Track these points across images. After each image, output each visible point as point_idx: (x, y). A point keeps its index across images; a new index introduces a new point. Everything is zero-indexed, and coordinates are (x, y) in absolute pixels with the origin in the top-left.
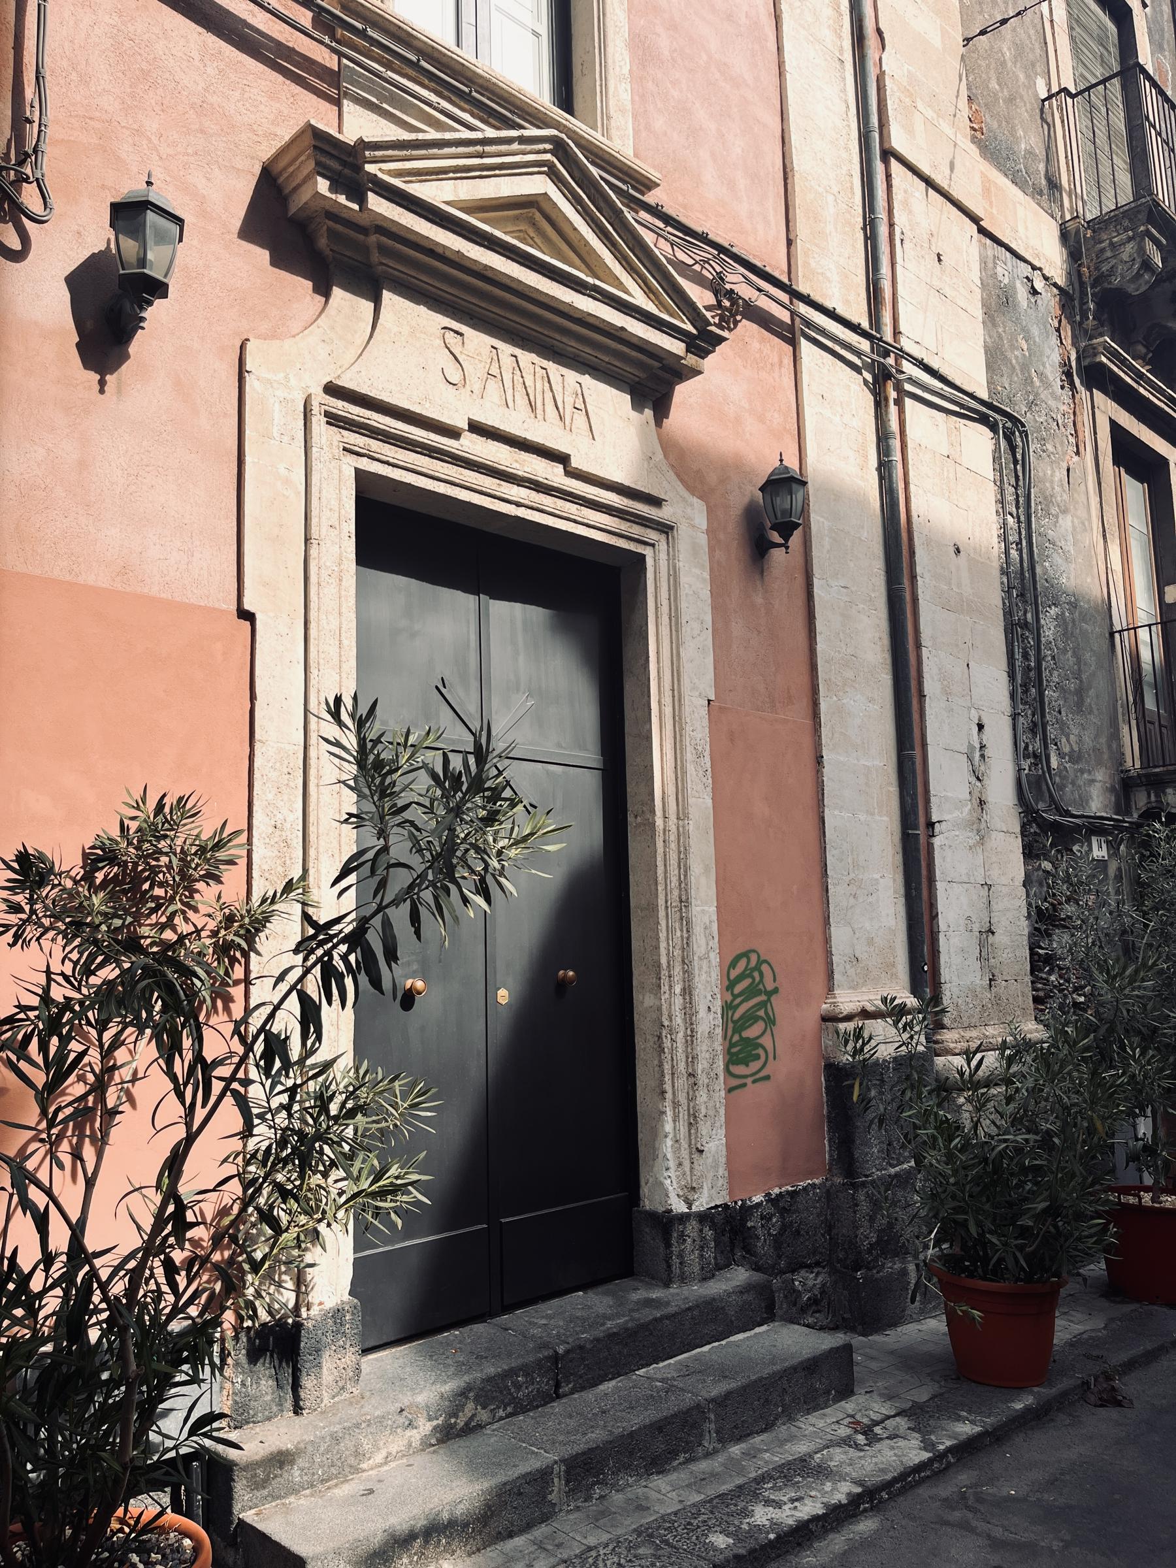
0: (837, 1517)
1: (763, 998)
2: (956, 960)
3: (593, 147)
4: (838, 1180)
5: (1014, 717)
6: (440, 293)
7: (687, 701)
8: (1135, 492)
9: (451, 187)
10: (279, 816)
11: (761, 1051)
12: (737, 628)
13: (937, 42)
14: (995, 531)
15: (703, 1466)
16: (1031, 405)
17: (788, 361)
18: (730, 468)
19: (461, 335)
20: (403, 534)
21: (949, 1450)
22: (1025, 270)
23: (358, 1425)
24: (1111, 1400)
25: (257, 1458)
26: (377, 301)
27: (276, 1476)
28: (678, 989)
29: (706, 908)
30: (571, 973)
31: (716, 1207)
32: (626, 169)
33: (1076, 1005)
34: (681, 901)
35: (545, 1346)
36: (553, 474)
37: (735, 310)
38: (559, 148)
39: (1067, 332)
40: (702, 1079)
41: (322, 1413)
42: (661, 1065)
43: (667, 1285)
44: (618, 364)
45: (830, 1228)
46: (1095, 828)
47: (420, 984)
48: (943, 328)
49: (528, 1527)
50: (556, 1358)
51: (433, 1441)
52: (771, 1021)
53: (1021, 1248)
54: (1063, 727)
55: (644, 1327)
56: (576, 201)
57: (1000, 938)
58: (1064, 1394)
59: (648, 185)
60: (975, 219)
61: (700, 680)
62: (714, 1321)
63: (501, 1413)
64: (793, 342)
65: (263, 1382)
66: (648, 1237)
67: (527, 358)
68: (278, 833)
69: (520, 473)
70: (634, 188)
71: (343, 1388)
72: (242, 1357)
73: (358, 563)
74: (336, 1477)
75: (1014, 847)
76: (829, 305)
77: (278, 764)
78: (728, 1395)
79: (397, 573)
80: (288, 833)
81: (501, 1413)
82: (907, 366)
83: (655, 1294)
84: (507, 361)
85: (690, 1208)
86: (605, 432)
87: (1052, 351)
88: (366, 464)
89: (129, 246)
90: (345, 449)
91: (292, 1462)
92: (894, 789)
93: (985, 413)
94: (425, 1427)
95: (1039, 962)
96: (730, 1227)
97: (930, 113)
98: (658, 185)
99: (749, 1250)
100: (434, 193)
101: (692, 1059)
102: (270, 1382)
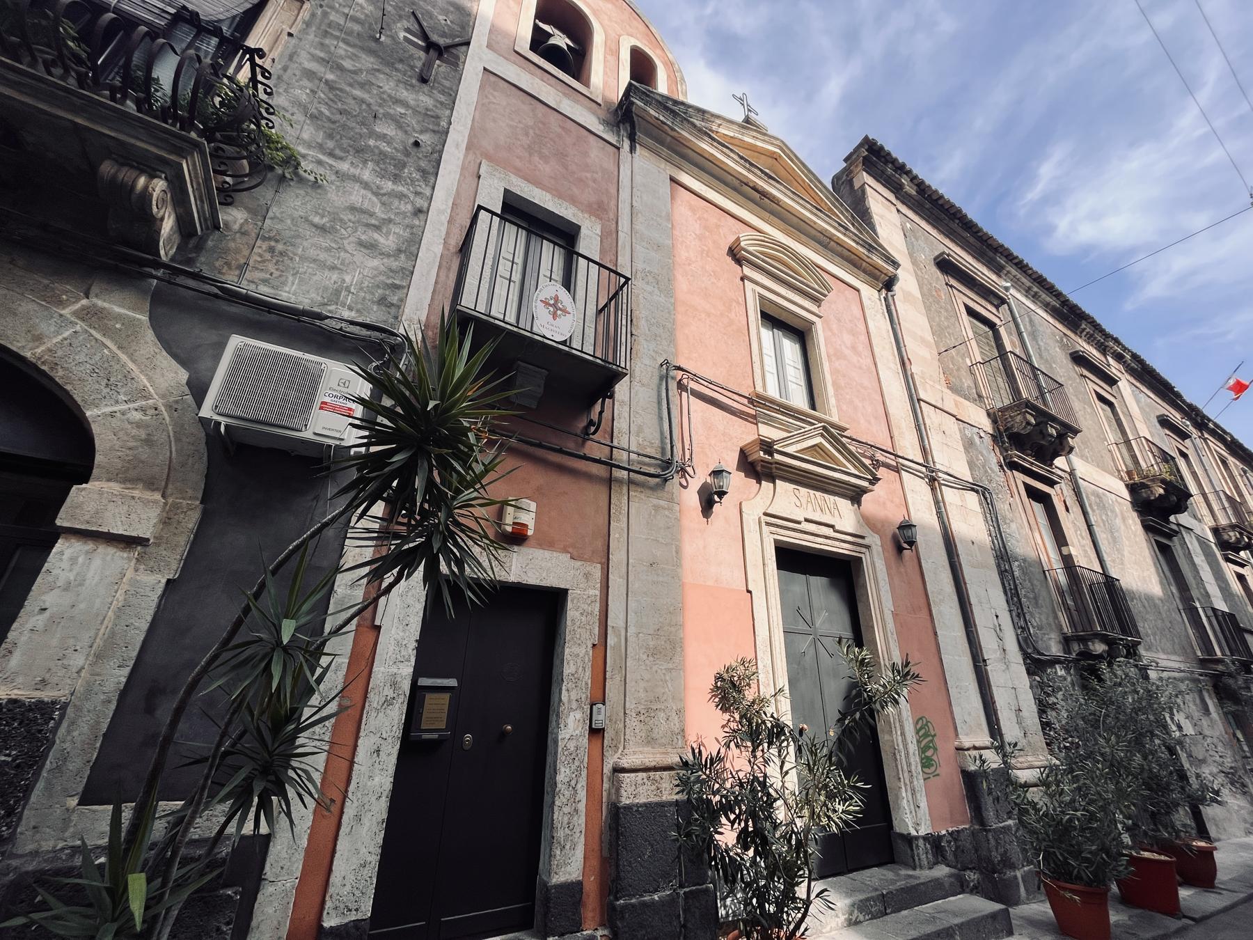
4: (977, 827)
5: (1010, 611)
8: (1038, 508)
9: (794, 445)
13: (928, 356)
16: (990, 481)
20: (792, 559)
22: (976, 430)
26: (774, 483)
33: (1065, 747)
35: (876, 890)
36: (829, 532)
37: (878, 464)
38: (824, 428)
39: (997, 450)
45: (976, 851)
46: (1054, 662)
48: (951, 459)
52: (935, 749)
55: (913, 887)
56: (830, 443)
57: (1025, 713)
59: (845, 430)
61: (888, 605)
66: (901, 846)
67: (818, 494)
73: (779, 568)
75: (1022, 670)
78: (962, 924)
82: (940, 474)
86: (844, 515)
87: (993, 458)
93: (973, 488)
95: (1046, 725)
96: (934, 842)
99: (944, 857)
100: (789, 450)
101: (909, 765)
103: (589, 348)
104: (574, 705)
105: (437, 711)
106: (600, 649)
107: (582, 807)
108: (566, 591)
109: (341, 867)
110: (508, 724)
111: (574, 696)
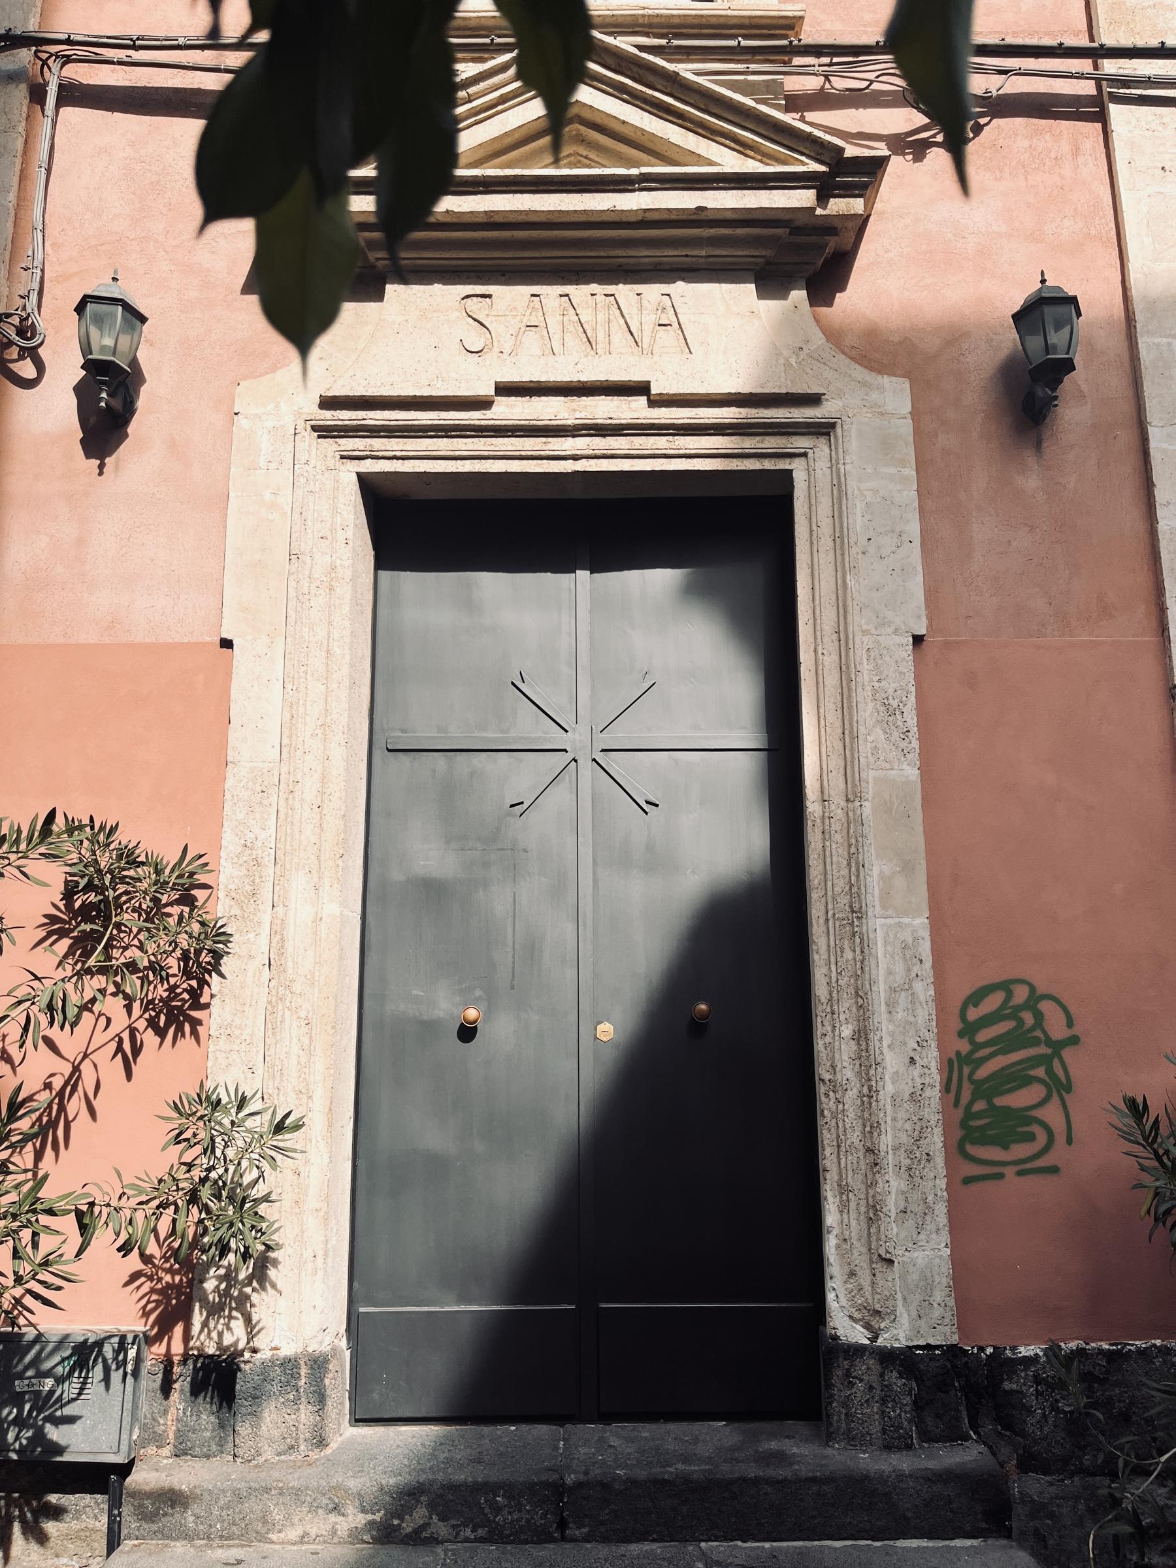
1: (1043, 1050)
3: (690, 20)
6: (454, 262)
10: (252, 835)
11: (1036, 1129)
18: (954, 336)
19: (489, 296)
23: (267, 1490)
25: (147, 1488)
27: (165, 1515)
28: (847, 1031)
29: (906, 920)
30: (703, 1007)
31: (928, 1347)
32: (747, 22)
34: (853, 912)
36: (634, 409)
41: (256, 1466)
43: (828, 1438)
44: (724, 253)
51: (367, 1538)
59: (791, 24)
63: (468, 1533)
64: (1102, 117)
65: (204, 1417)
67: (580, 292)
68: (248, 852)
69: (569, 422)
70: (745, 37)
71: (292, 1447)
72: (187, 1388)
74: (238, 1538)
77: (250, 784)
79: (503, 571)
80: (260, 852)
81: (468, 1533)
85: (874, 1339)
86: (715, 339)
88: (369, 466)
89: (1035, 343)
90: (342, 457)
91: (186, 1506)
94: (355, 1519)
96: (951, 1384)
98: (802, 18)
101: (871, 1128)
102: (212, 1418)
103: (458, 14)
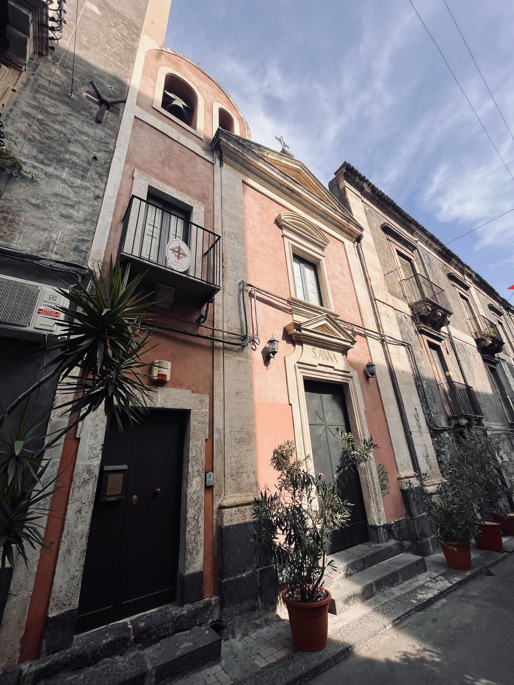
0: (437, 598)
2: (422, 463)
4: (409, 518)
5: (422, 406)
7: (361, 411)
8: (434, 352)
9: (312, 325)
12: (366, 394)
13: (379, 276)
14: (410, 367)
15: (401, 586)
16: (411, 340)
17: (365, 341)
18: (359, 364)
20: (312, 386)
21: (456, 584)
22: (403, 314)
24: (489, 574)
26: (302, 346)
33: (450, 473)
35: (360, 556)
37: (355, 334)
40: (378, 494)
42: (369, 491)
45: (409, 530)
46: (444, 430)
47: (322, 474)
48: (391, 330)
49: (371, 597)
50: (363, 559)
52: (388, 480)
53: (460, 533)
54: (432, 407)
56: (330, 323)
57: (430, 457)
58: (477, 572)
60: (393, 307)
61: (362, 407)
62: (389, 553)
76: (371, 330)
78: (402, 569)
82: (386, 338)
83: (377, 545)
84: (322, 352)
86: (338, 361)
87: (412, 328)
92: (402, 425)
93: (403, 344)
95: (440, 463)
97: (381, 290)
99: (393, 535)
100: (309, 328)
101: (375, 489)
104: (196, 474)
105: (115, 485)
106: (210, 442)
107: (202, 530)
108: (189, 411)
109: (59, 581)
110: (159, 488)
111: (195, 468)
